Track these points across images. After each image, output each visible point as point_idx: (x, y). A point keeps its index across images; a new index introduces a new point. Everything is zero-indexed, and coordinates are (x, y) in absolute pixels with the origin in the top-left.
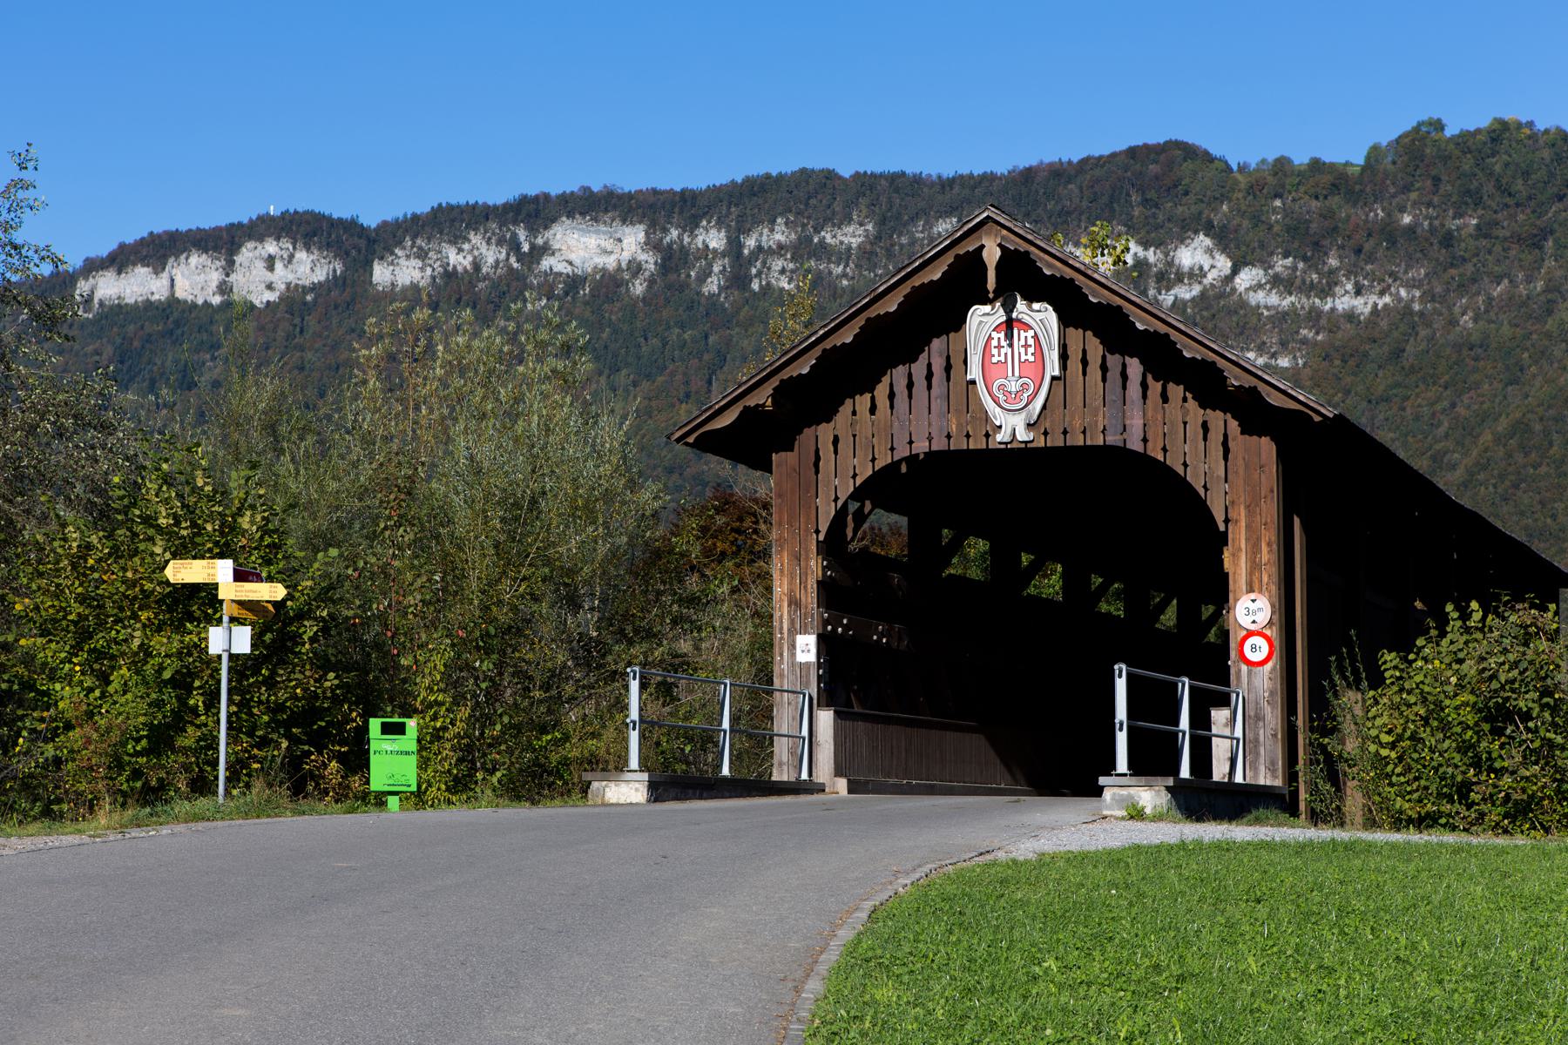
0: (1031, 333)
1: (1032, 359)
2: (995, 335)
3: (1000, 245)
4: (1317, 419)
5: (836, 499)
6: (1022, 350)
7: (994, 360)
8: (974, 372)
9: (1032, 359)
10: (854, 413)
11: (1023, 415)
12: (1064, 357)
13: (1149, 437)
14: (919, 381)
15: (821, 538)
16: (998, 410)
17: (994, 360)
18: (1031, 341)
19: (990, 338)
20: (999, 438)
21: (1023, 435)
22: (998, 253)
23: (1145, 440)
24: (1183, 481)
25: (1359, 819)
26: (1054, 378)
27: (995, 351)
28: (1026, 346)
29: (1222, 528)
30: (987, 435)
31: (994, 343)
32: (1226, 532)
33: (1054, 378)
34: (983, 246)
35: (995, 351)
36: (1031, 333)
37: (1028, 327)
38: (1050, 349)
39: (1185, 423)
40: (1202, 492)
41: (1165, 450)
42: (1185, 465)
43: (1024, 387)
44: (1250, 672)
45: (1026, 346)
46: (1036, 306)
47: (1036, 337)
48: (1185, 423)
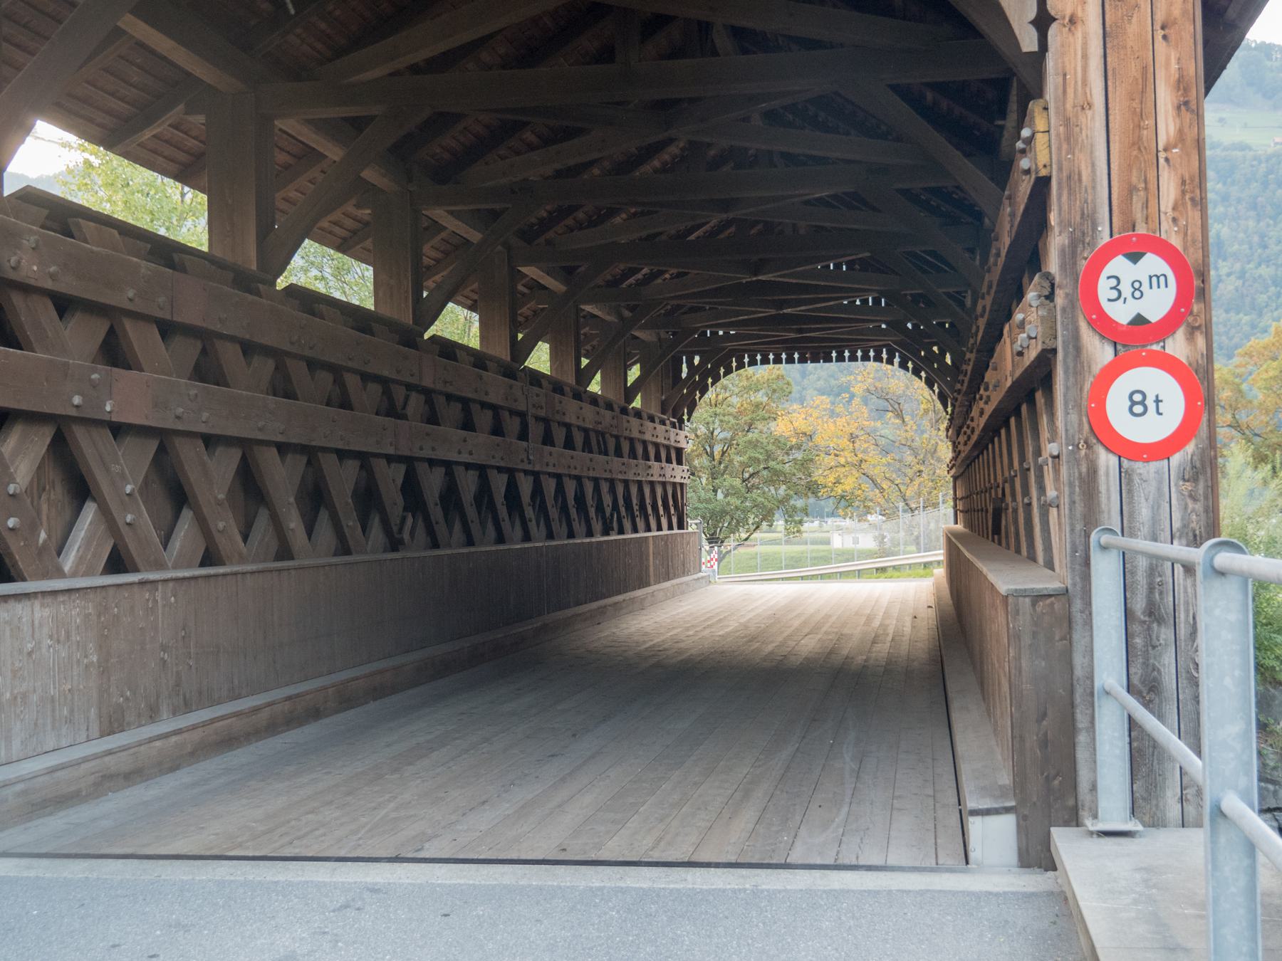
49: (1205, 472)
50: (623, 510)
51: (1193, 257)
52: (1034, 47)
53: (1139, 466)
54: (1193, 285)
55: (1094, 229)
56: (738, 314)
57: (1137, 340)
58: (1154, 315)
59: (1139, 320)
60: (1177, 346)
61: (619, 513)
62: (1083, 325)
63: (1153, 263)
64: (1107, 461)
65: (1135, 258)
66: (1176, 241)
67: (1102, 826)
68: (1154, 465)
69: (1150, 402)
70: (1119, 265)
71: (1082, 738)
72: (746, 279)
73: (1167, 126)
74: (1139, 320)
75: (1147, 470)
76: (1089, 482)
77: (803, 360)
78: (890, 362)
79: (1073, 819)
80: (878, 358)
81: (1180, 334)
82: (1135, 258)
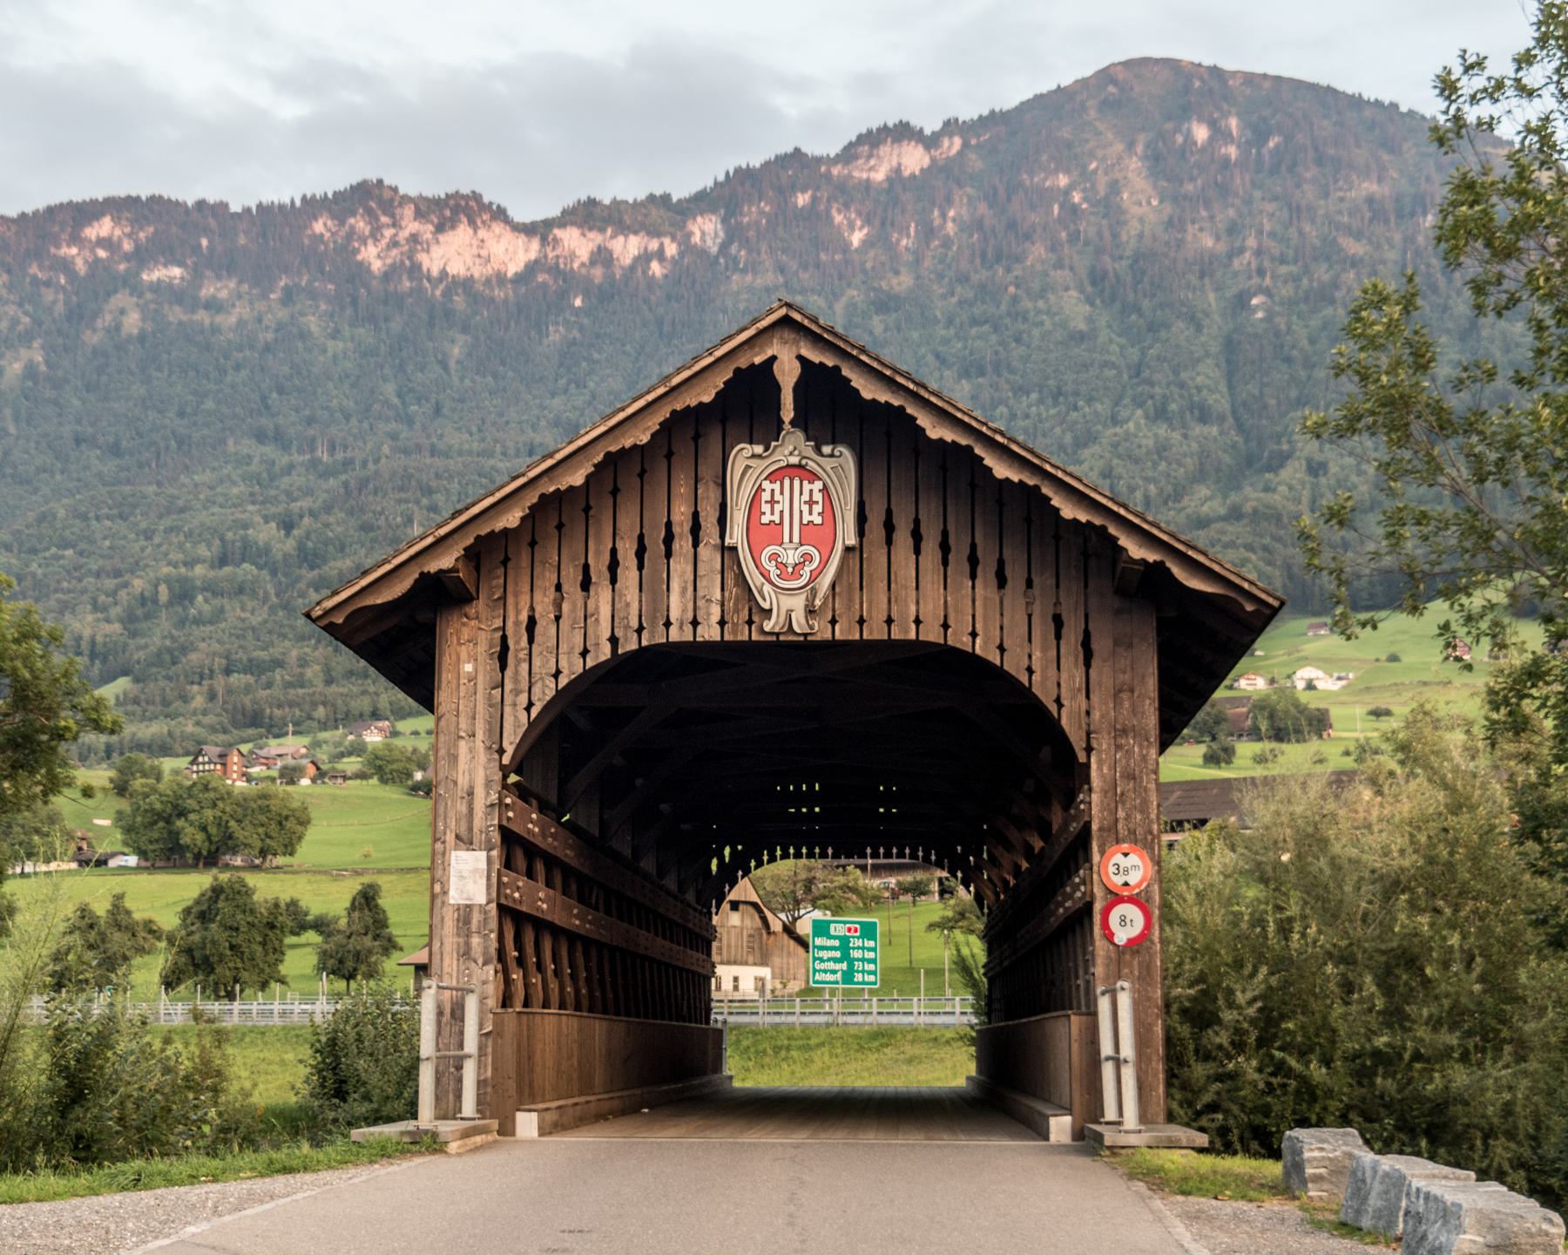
0: (818, 485)
1: (818, 520)
2: (767, 485)
4: (1249, 608)
6: (805, 508)
9: (818, 520)
12: (861, 519)
13: (951, 622)
14: (627, 551)
16: (767, 588)
17: (765, 519)
18: (818, 497)
19: (760, 489)
22: (796, 369)
23: (946, 626)
24: (1026, 693)
25: (1161, 1118)
26: (848, 549)
28: (811, 503)
29: (1082, 758)
31: (766, 496)
32: (1087, 765)
33: (848, 549)
35: (766, 508)
36: (818, 485)
40: (1053, 708)
41: (1001, 648)
43: (807, 557)
47: (825, 489)
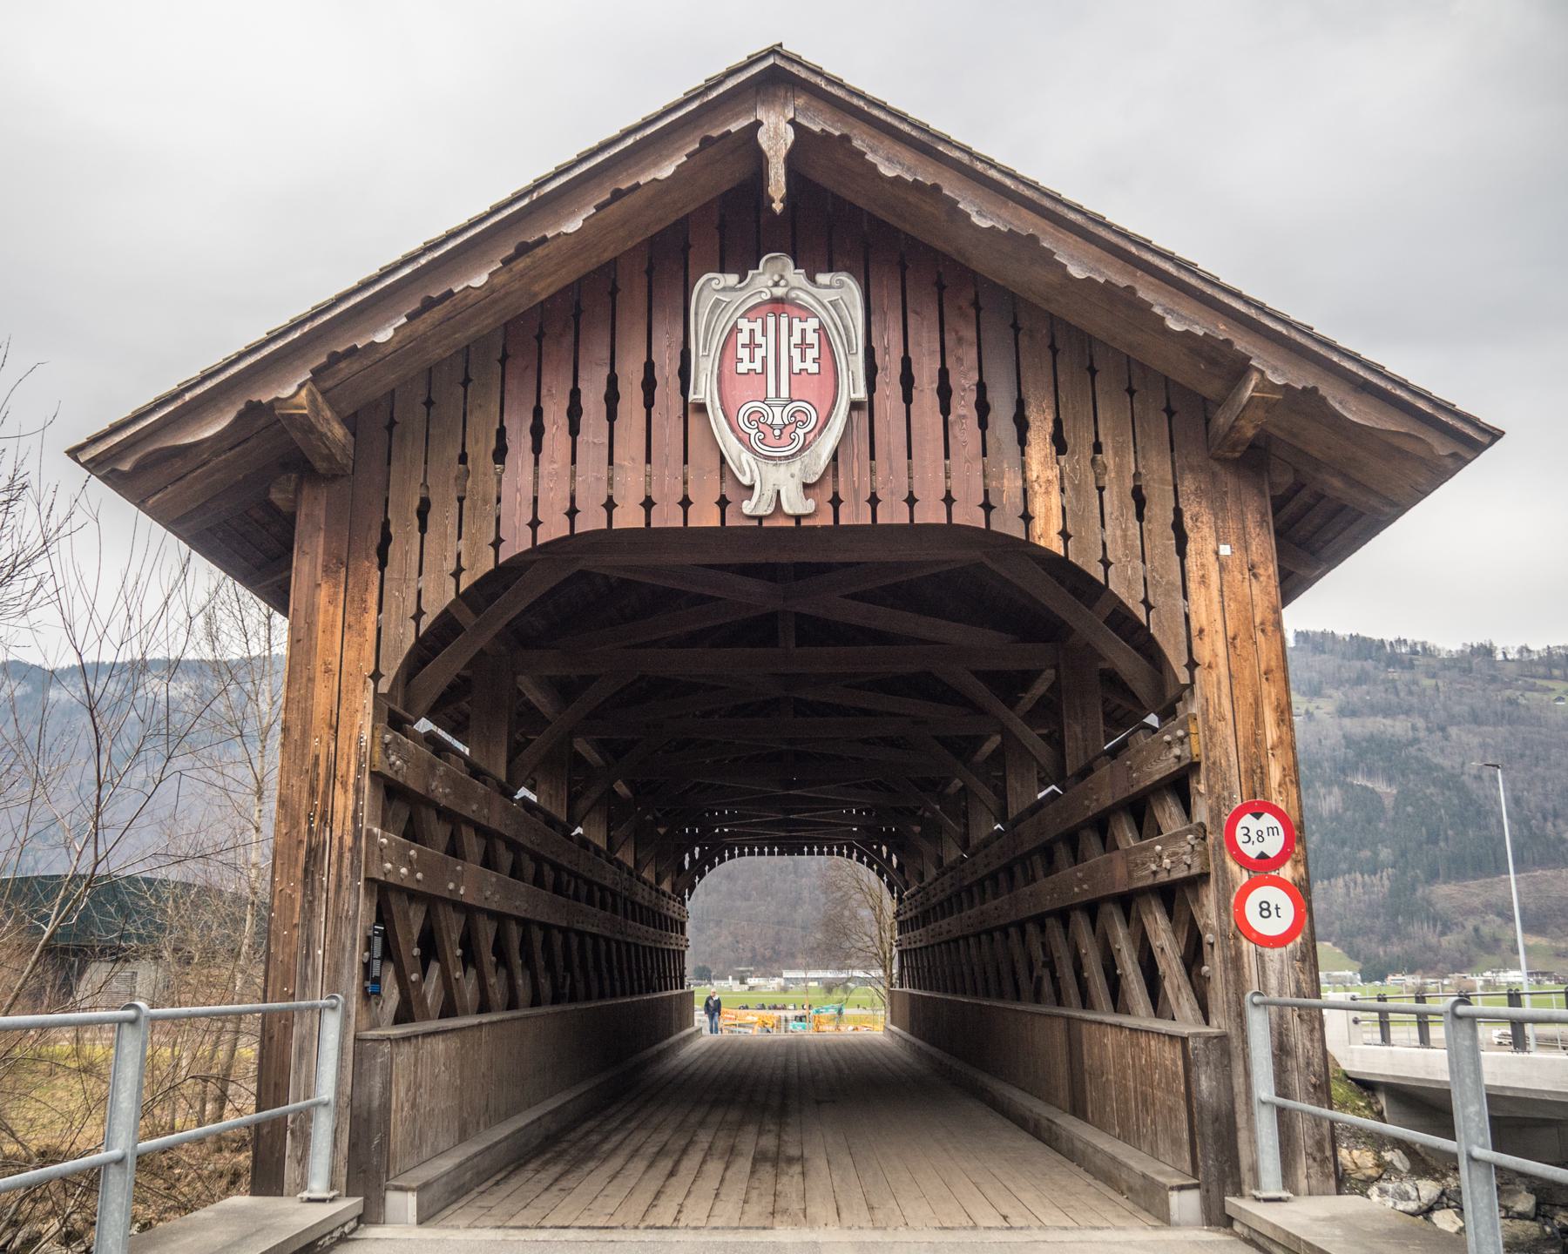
0: (813, 323)
1: (814, 368)
2: (744, 324)
3: (792, 122)
5: (418, 616)
7: (742, 368)
8: (704, 389)
9: (814, 368)
10: (463, 459)
11: (796, 467)
15: (384, 687)
16: (746, 456)
17: (742, 368)
18: (812, 338)
19: (735, 329)
20: (748, 507)
21: (796, 503)
22: (790, 135)
26: (855, 406)
27: (744, 353)
28: (752, 345)
30: (723, 502)
31: (743, 338)
33: (855, 406)
34: (758, 124)
35: (744, 353)
36: (813, 323)
37: (806, 312)
38: (849, 352)
39: (1101, 489)
40: (1141, 613)
42: (1106, 564)
43: (795, 421)
44: (1260, 956)
45: (803, 346)
46: (823, 278)
47: (821, 330)
48: (1101, 489)
49: (1309, 958)
50: (577, 972)
51: (1294, 816)
52: (1188, 682)
53: (1268, 951)
54: (1294, 833)
55: (1231, 795)
56: (752, 817)
57: (1262, 867)
58: (1272, 853)
59: (1262, 856)
60: (1287, 872)
61: (573, 977)
62: (1228, 859)
63: (1268, 820)
64: (1247, 947)
65: (1257, 816)
66: (1282, 806)
67: (1264, 1195)
68: (1278, 951)
69: (1272, 909)
70: (1247, 820)
71: (1243, 1136)
72: (781, 792)
73: (1271, 734)
74: (1262, 856)
75: (1273, 954)
76: (1236, 962)
77: (781, 853)
78: (849, 856)
79: (1238, 1192)
80: (840, 853)
81: (1288, 864)
82: (1257, 816)
